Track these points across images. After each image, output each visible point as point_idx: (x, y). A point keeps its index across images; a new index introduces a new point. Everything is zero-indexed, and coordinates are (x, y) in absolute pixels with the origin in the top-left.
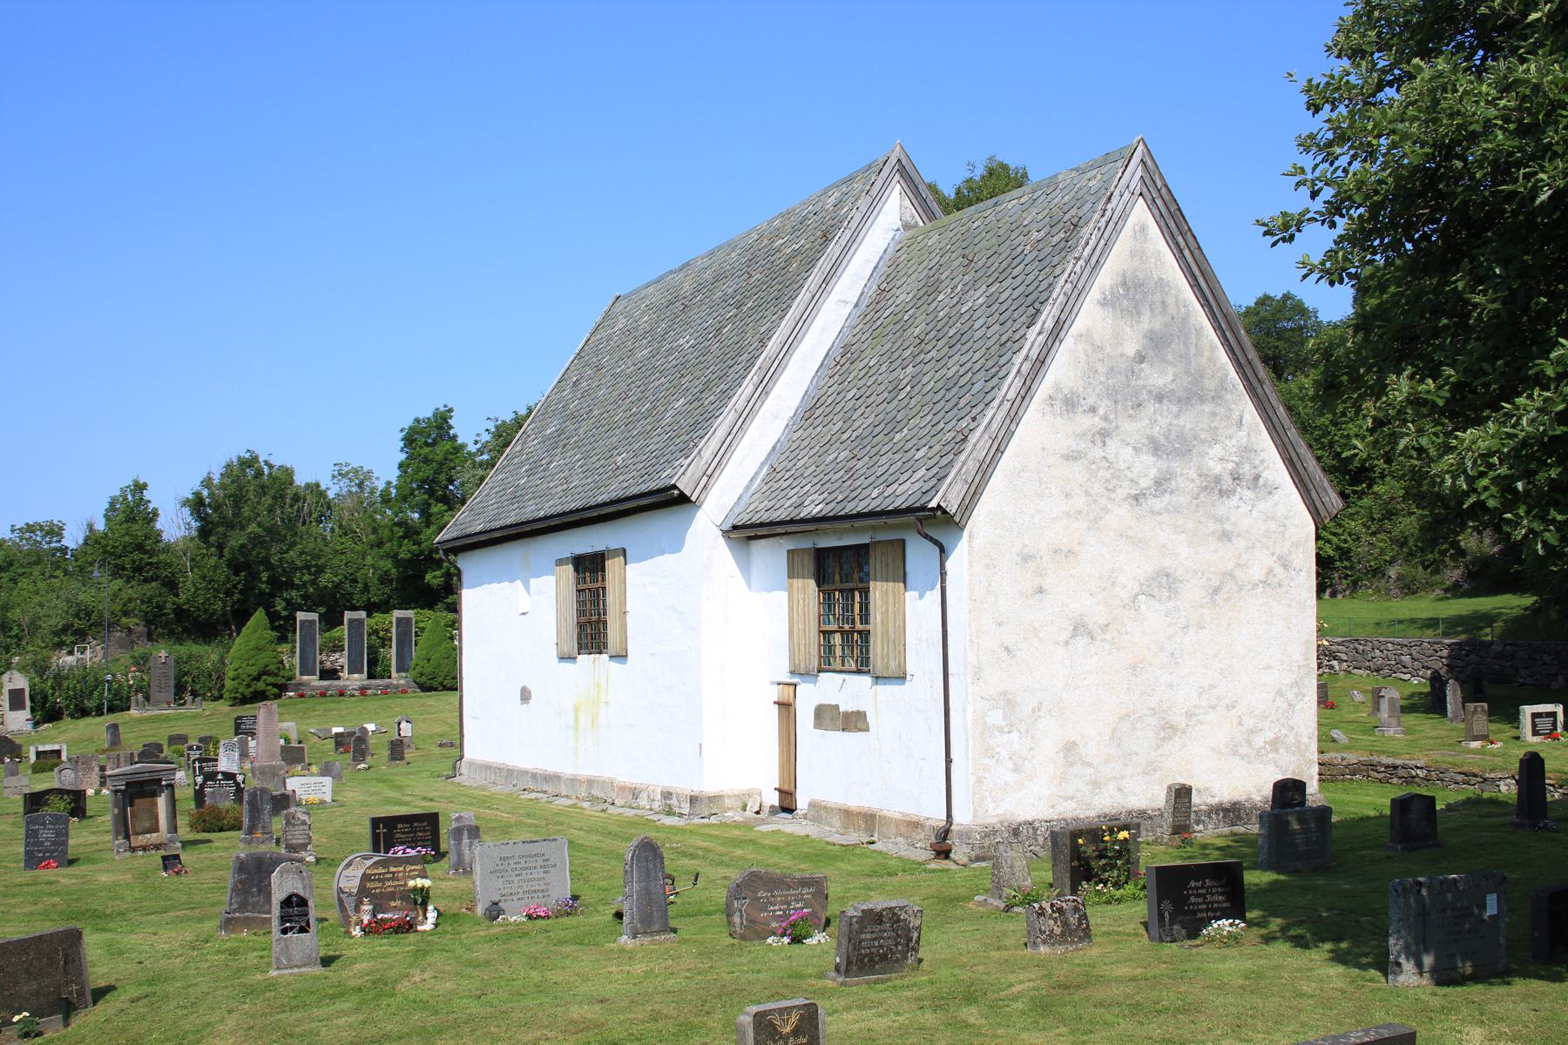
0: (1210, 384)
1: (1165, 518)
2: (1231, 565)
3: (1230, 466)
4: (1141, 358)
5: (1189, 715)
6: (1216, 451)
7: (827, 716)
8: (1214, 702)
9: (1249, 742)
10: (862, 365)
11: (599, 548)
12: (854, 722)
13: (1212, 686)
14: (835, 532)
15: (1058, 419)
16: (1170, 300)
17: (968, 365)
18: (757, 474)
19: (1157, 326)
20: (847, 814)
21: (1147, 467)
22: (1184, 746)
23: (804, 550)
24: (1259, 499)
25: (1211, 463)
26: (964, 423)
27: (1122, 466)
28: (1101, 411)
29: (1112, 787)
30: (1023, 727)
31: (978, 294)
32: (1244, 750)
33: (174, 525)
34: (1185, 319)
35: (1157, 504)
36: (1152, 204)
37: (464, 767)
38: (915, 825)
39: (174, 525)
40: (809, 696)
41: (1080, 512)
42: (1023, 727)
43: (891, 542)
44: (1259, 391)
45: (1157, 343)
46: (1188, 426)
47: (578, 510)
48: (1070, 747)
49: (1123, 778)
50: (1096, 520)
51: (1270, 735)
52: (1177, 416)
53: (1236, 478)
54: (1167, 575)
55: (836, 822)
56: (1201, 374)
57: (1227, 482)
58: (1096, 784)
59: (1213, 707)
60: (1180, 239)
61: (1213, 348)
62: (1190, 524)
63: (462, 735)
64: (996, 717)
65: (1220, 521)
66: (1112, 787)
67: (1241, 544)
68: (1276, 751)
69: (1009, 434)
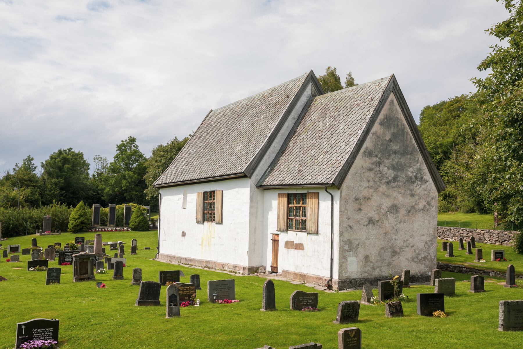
0: (410, 149)
1: (395, 189)
2: (414, 204)
3: (415, 174)
4: (390, 141)
5: (401, 249)
6: (411, 169)
7: (289, 245)
8: (408, 245)
9: (417, 258)
10: (301, 138)
11: (213, 189)
12: (299, 247)
13: (407, 240)
14: (294, 189)
15: (367, 158)
16: (399, 124)
17: (339, 140)
18: (267, 170)
19: (395, 131)
20: (295, 275)
21: (391, 174)
22: (399, 258)
23: (284, 194)
24: (422, 184)
25: (409, 173)
26: (339, 158)
27: (384, 173)
28: (379, 156)
29: (378, 269)
30: (354, 250)
31: (340, 119)
32: (416, 260)
33: (39, 172)
34: (403, 130)
35: (394, 185)
36: (395, 95)
37: (159, 256)
38: (320, 278)
39: (39, 172)
40: (283, 238)
41: (372, 186)
42: (354, 250)
43: (314, 193)
44: (424, 152)
45: (395, 137)
46: (403, 162)
47: (207, 178)
48: (367, 257)
49: (381, 267)
50: (376, 189)
51: (423, 256)
52: (400, 159)
53: (416, 178)
54: (396, 206)
55: (292, 277)
56: (407, 146)
57: (414, 179)
58: (374, 269)
59: (408, 247)
60: (403, 105)
61: (411, 139)
62: (403, 191)
63: (159, 246)
64: (346, 247)
65: (411, 190)
66: (378, 269)
67: (417, 197)
68: (425, 261)
69: (353, 162)
